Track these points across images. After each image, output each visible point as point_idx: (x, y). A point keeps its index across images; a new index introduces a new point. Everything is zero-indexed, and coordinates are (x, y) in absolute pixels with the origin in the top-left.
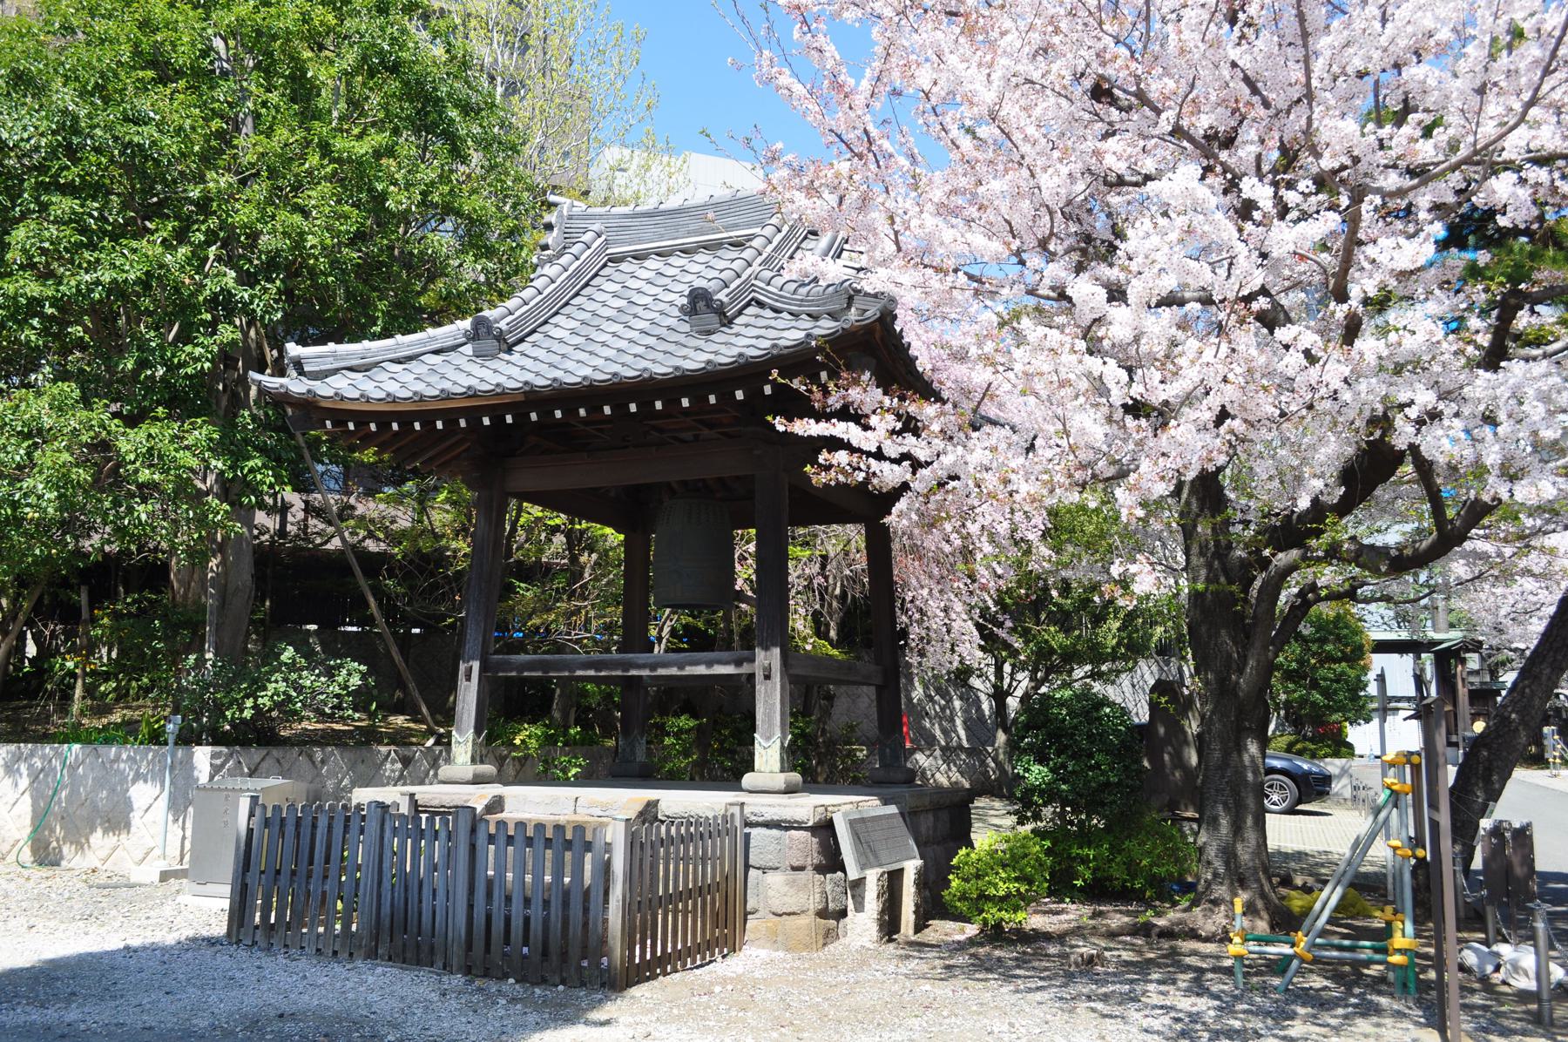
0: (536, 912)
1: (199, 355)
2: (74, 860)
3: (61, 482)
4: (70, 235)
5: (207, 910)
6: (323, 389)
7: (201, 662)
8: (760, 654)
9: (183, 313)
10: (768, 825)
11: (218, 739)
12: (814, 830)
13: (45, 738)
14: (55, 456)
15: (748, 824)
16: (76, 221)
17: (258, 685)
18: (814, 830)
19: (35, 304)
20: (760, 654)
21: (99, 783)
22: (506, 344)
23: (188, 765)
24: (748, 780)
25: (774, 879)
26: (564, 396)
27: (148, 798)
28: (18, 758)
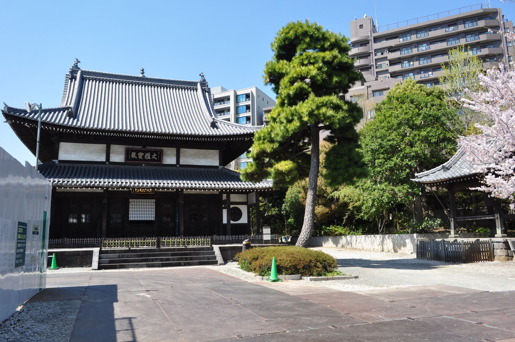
0: (451, 254)
1: (404, 175)
2: (400, 251)
3: (388, 197)
4: (383, 160)
5: (414, 256)
6: (421, 180)
7: (413, 221)
8: (496, 215)
9: (401, 168)
10: (497, 242)
11: (417, 232)
12: (504, 243)
13: (393, 234)
14: (386, 194)
15: (493, 242)
16: (384, 158)
17: (421, 224)
18: (504, 243)
19: (380, 172)
20: (496, 215)
21: (401, 240)
22: (448, 169)
23: (413, 236)
24: (496, 236)
25: (498, 251)
26: (453, 179)
27: (408, 241)
28: (389, 236)
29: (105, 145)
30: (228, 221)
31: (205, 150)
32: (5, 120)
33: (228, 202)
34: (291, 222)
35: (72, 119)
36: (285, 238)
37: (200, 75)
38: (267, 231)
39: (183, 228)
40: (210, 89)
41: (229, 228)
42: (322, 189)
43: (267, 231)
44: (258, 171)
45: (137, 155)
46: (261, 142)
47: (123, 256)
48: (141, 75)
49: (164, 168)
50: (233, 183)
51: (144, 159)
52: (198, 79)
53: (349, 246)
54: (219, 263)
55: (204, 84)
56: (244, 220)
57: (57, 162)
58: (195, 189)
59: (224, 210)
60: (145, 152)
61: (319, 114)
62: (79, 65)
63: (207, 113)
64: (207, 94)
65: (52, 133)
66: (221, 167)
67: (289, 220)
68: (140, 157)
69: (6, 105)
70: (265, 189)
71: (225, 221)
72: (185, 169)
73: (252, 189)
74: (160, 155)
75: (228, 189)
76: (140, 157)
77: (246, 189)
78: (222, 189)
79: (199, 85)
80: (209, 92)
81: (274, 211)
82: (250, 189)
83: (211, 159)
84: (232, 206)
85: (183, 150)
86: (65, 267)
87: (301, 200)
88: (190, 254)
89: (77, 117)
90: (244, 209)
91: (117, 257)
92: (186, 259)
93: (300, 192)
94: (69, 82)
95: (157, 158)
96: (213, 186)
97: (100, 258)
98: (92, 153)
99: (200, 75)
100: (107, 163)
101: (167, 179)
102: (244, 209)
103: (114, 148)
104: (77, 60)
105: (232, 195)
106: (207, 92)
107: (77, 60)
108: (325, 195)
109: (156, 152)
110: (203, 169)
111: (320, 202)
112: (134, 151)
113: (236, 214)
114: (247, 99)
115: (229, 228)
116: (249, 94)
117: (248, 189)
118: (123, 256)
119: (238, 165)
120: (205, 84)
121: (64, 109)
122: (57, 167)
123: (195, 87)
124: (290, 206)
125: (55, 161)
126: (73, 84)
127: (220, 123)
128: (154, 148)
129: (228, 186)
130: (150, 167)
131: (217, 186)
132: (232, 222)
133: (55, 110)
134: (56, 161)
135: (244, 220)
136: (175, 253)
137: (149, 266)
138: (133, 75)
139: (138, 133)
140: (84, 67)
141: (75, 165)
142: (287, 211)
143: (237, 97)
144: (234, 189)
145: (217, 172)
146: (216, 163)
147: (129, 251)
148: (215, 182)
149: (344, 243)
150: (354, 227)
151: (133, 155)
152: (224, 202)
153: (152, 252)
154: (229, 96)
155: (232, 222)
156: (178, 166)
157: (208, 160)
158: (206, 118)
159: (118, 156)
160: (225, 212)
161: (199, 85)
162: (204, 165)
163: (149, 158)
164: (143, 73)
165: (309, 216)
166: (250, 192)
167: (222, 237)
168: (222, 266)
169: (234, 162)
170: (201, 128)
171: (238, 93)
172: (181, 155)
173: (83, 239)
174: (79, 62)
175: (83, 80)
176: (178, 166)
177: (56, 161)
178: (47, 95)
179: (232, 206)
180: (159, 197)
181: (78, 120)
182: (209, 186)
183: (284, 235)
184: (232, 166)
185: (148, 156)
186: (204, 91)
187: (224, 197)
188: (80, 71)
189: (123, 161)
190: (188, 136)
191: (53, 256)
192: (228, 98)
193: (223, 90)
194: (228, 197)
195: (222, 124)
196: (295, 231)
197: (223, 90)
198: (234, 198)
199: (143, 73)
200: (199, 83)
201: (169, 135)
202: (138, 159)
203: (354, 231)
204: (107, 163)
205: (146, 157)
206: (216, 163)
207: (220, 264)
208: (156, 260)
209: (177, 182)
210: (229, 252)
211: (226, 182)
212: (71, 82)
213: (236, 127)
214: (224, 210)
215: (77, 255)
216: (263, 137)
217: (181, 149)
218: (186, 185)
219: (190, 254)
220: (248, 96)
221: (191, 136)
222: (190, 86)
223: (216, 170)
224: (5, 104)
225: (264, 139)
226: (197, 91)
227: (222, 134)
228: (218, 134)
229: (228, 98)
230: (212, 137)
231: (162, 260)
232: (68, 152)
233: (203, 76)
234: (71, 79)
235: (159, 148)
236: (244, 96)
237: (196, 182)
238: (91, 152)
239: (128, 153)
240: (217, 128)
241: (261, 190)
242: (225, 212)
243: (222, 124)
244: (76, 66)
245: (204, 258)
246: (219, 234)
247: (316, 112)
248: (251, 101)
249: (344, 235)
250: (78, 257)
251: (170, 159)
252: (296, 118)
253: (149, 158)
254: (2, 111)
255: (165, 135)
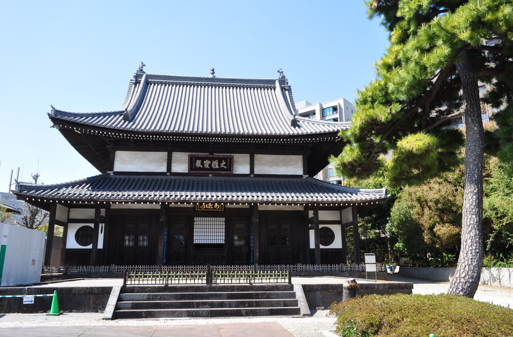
29: (166, 153)
30: (317, 245)
31: (285, 156)
32: (52, 124)
33: (315, 221)
34: (399, 247)
35: (127, 122)
36: (390, 268)
37: (278, 71)
38: (370, 259)
39: (258, 254)
40: (290, 87)
41: (317, 254)
42: (449, 200)
43: (370, 259)
44: (363, 160)
45: (202, 164)
46: (369, 105)
47: (155, 298)
48: (211, 76)
49: (235, 179)
50: (321, 194)
51: (211, 168)
52: (276, 76)
53: (497, 283)
54: (302, 312)
55: (283, 81)
56: (337, 244)
57: (112, 174)
58: (273, 203)
59: (310, 231)
60: (212, 159)
61: (497, 20)
62: (144, 69)
63: (287, 111)
64: (287, 92)
65: (107, 140)
66: (305, 176)
67: (397, 245)
68: (207, 166)
69: (53, 108)
70: (364, 202)
71: (312, 246)
72: (261, 179)
73: (347, 202)
74: (230, 163)
75: (315, 203)
76: (207, 166)
77: (339, 203)
78: (307, 203)
79: (277, 83)
80: (289, 90)
81: (372, 234)
82: (344, 203)
83: (293, 166)
84: (321, 226)
85: (257, 157)
86: (71, 312)
87: (415, 217)
88: (257, 296)
89: (134, 121)
90: (337, 230)
91: (145, 298)
92: (250, 304)
93: (412, 207)
94: (133, 87)
95: (227, 166)
96: (295, 199)
97: (120, 299)
98: (151, 163)
99: (278, 71)
100: (168, 174)
101: (237, 191)
102: (337, 230)
103: (176, 155)
104: (142, 63)
105: (320, 212)
106: (287, 90)
107: (142, 63)
108: (454, 209)
109: (225, 159)
110: (283, 180)
111: (445, 219)
112: (199, 158)
113: (326, 236)
114: (335, 112)
115: (317, 254)
116: (337, 106)
117: (342, 202)
118: (155, 298)
119: (326, 175)
120: (284, 81)
121: (120, 113)
122: (111, 179)
123: (273, 85)
124: (398, 227)
125: (109, 172)
126: (136, 89)
127: (304, 122)
128: (222, 155)
129: (315, 199)
130: (218, 178)
131: (300, 199)
132: (322, 247)
133: (110, 114)
134: (111, 173)
135: (337, 244)
136: (234, 292)
137: (191, 315)
138: (202, 76)
139: (202, 135)
140: (149, 71)
141: (132, 177)
142: (393, 233)
143: (323, 110)
144: (323, 203)
145: (301, 182)
146: (299, 171)
147: (166, 288)
148: (298, 194)
149: (486, 279)
150: (501, 255)
151: (198, 164)
152: (311, 221)
153: (199, 291)
154: (314, 110)
155: (322, 247)
156: (252, 176)
157: (288, 168)
158: (285, 117)
159: (181, 165)
160: (312, 233)
161: (277, 83)
162: (284, 174)
163: (217, 167)
164: (213, 73)
165: (472, 234)
166: (344, 207)
167: (309, 267)
168: (307, 319)
169: (321, 172)
170: (280, 126)
171: (324, 106)
172: (255, 162)
173: (133, 267)
174: (144, 65)
175: (147, 84)
176: (252, 176)
177: (111, 173)
178: (104, 99)
179: (321, 226)
180: (231, 215)
181: (134, 123)
182: (290, 199)
183: (388, 263)
184: (320, 176)
185: (215, 164)
186: (283, 89)
187: (311, 214)
188: (145, 75)
189: (187, 172)
190: (262, 136)
191: (54, 295)
192: (314, 113)
193: (308, 104)
194: (316, 214)
195: (306, 123)
196: (404, 259)
197: (308, 104)
198: (323, 215)
199: (213, 73)
200: (277, 81)
201: (239, 136)
202: (204, 169)
203: (502, 260)
204: (168, 174)
205: (213, 166)
206: (299, 171)
207: (304, 315)
208: (204, 304)
209: (249, 194)
210: (318, 294)
211: (312, 194)
212: (135, 87)
213: (324, 125)
214: (310, 231)
215: (90, 293)
216: (372, 97)
217: (255, 155)
218: (260, 198)
219: (257, 296)
220: (335, 109)
221: (267, 136)
222: (267, 84)
223: (299, 180)
224: (52, 107)
225: (373, 102)
226: (275, 90)
227: (305, 132)
228: (300, 133)
229: (314, 113)
230: (293, 136)
231: (212, 305)
232: (126, 162)
233: (282, 72)
234: (135, 84)
235: (229, 155)
236: (331, 109)
237: (273, 194)
238: (150, 162)
239: (192, 161)
240: (299, 127)
241: (359, 204)
242: (312, 233)
243: (306, 123)
244: (141, 70)
245: (278, 304)
246: (305, 263)
247: (489, 17)
248: (338, 114)
249: (486, 266)
250: (92, 296)
251: (241, 167)
252: (440, 42)
253: (217, 167)
254: (49, 114)
255: (234, 136)
